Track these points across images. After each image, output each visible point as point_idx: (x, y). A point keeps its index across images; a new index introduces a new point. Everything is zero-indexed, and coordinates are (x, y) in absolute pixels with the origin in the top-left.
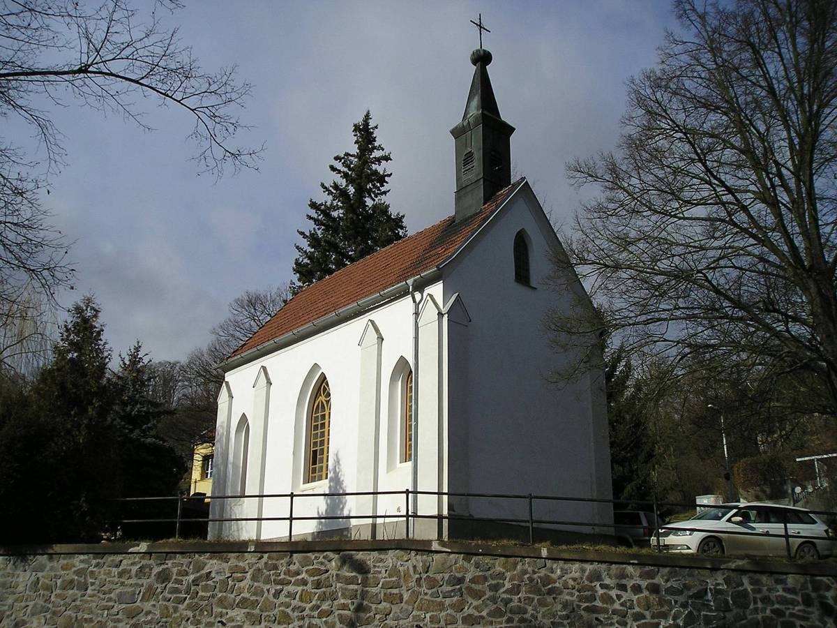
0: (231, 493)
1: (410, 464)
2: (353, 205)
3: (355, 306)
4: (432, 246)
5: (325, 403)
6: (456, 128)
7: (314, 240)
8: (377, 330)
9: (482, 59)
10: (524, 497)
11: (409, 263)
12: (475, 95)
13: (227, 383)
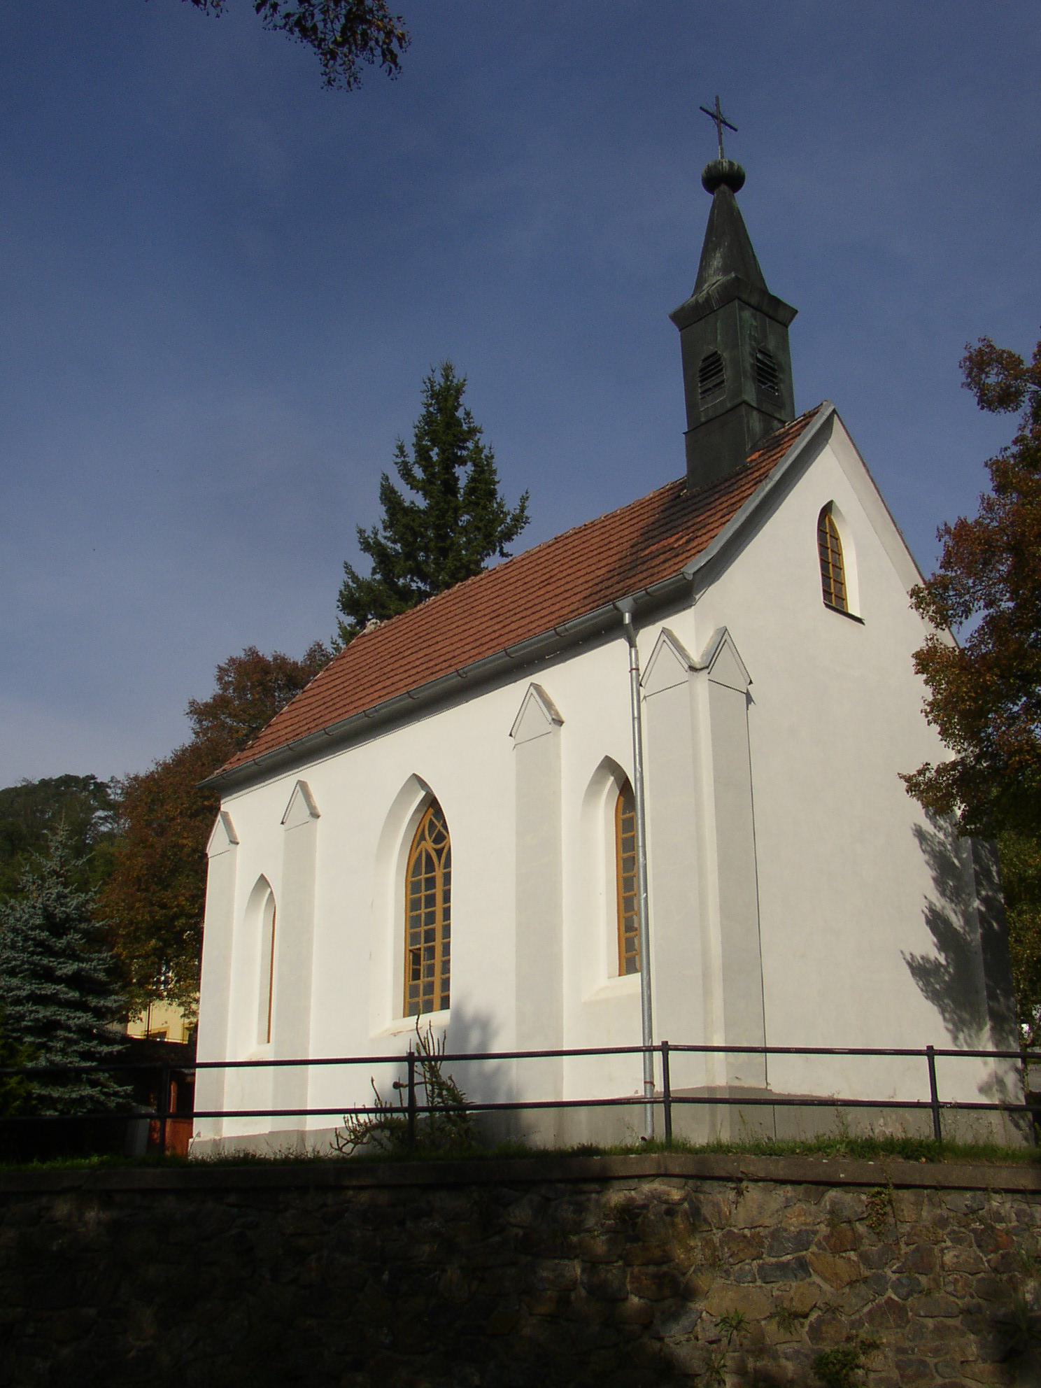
0: (729, 1026)
1: (636, 977)
2: (439, 484)
3: (550, 637)
4: (651, 534)
5: (434, 854)
6: (682, 308)
7: (495, 483)
8: (549, 704)
9: (724, 181)
10: (918, 1053)
11: (603, 570)
12: (714, 250)
13: (225, 815)
